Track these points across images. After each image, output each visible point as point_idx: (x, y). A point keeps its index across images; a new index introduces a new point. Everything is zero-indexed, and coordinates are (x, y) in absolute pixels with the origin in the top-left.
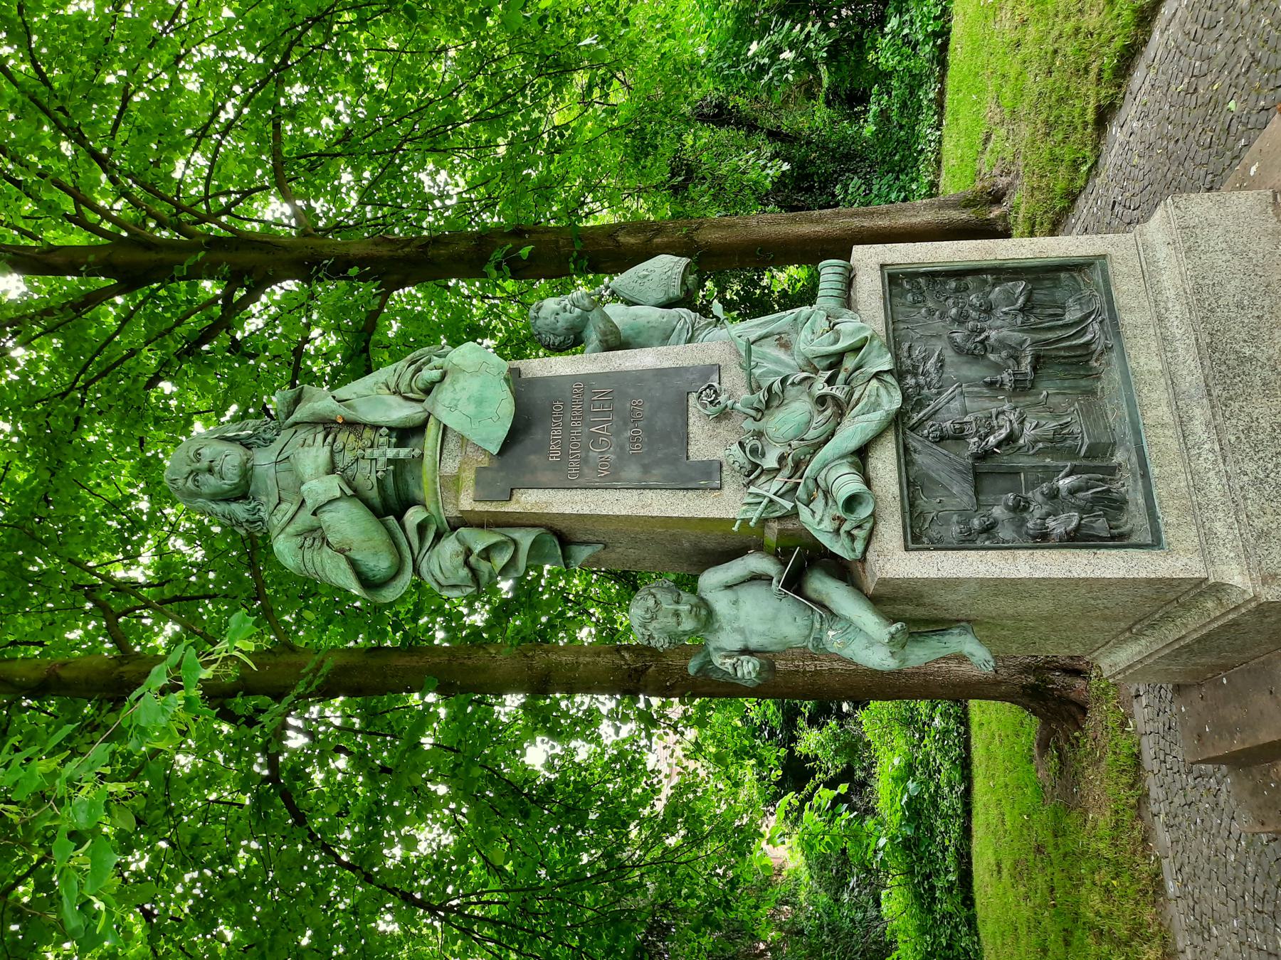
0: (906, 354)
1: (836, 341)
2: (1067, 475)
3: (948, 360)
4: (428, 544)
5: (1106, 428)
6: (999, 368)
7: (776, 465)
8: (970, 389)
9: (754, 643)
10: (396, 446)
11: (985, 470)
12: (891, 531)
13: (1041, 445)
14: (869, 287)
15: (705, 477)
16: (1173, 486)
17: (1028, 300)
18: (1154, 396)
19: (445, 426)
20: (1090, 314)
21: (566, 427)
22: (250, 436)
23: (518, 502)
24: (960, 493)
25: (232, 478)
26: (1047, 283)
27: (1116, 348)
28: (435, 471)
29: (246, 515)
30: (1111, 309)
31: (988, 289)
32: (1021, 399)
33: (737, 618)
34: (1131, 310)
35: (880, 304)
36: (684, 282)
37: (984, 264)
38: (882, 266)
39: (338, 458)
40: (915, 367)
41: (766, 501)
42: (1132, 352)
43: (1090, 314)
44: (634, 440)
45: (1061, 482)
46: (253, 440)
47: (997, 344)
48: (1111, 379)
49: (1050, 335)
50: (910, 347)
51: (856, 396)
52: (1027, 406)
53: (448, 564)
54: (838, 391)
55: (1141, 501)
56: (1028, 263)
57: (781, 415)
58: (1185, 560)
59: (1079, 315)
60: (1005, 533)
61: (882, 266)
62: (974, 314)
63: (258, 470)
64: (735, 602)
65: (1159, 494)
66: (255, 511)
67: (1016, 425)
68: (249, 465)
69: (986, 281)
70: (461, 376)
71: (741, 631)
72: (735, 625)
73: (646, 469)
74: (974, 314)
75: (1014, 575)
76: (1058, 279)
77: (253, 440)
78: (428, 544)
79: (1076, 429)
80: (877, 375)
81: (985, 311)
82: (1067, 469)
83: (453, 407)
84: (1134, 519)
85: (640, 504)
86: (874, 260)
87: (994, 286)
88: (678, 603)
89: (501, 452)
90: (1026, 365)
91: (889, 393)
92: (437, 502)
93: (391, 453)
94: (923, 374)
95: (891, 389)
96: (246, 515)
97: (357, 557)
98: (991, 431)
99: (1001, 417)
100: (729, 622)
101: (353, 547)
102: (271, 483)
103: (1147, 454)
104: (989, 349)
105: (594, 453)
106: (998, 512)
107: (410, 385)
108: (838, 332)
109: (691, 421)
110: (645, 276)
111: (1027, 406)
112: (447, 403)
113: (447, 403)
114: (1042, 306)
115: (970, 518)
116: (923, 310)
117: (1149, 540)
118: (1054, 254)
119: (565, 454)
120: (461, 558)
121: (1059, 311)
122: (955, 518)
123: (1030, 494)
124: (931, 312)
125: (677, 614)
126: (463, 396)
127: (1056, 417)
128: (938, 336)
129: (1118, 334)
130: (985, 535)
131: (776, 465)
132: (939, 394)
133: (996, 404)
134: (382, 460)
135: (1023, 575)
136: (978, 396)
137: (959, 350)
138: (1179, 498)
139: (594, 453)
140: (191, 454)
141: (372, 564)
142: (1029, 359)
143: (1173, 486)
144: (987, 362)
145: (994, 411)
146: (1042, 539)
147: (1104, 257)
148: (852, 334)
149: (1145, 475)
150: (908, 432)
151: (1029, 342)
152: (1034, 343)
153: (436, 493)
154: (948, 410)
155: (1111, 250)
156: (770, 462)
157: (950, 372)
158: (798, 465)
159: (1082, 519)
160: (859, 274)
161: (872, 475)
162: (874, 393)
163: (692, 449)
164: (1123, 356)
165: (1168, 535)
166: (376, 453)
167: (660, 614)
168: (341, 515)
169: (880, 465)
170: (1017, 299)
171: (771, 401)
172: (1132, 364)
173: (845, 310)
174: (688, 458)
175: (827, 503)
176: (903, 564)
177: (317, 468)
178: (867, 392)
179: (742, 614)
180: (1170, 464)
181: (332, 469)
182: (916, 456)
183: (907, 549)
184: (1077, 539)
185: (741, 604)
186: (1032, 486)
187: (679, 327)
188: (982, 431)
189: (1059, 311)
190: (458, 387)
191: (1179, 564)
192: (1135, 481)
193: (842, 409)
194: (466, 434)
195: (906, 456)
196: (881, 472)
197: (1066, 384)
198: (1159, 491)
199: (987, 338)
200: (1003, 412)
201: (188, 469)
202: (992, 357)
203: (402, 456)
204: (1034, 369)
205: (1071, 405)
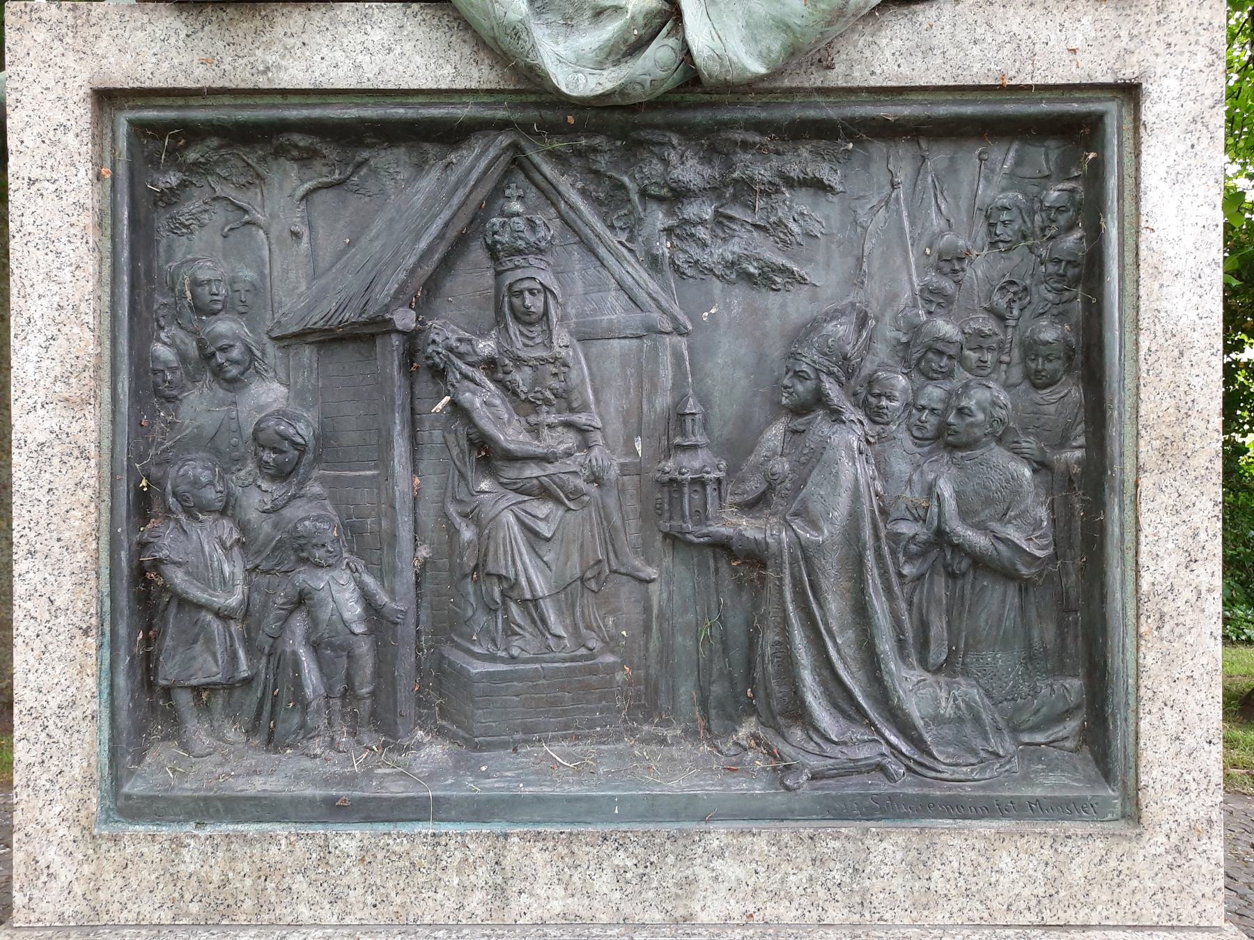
0: (794, 171)
2: (367, 598)
3: (772, 301)
5: (528, 730)
13: (467, 534)
16: (300, 884)
17: (979, 562)
18: (603, 882)
20: (917, 742)
26: (1045, 633)
27: (780, 799)
30: (925, 808)
31: (1029, 444)
32: (632, 504)
34: (918, 866)
35: (978, 71)
37: (1119, 432)
38: (1130, 92)
42: (761, 843)
43: (917, 742)
45: (344, 577)
47: (811, 440)
48: (681, 768)
49: (835, 606)
52: (605, 516)
55: (258, 785)
56: (1115, 573)
58: (65, 875)
59: (914, 709)
61: (1130, 92)
65: (273, 839)
67: (532, 471)
69: (1063, 443)
76: (1061, 670)
81: (943, 429)
82: (383, 598)
84: (217, 755)
87: (1041, 467)
98: (524, 404)
103: (405, 828)
104: (799, 423)
111: (605, 516)
114: (954, 610)
117: (134, 787)
118: (1149, 659)
121: (938, 654)
124: (951, 262)
128: (858, 277)
129: (840, 811)
130: (192, 349)
132: (654, 263)
133: (616, 427)
136: (645, 378)
138: (260, 893)
142: (750, 534)
143: (300, 884)
144: (759, 413)
146: (142, 498)
147: (1132, 813)
149: (334, 811)
151: (806, 535)
152: (806, 555)
154: (601, 286)
155: (1156, 842)
157: (727, 304)
164: (748, 813)
165: (143, 841)
170: (981, 527)
172: (719, 835)
176: (48, 79)
180: (369, 888)
184: (144, 601)
189: (938, 654)
191: (51, 855)
192: (326, 782)
197: (682, 641)
198: (284, 843)
199: (836, 415)
200: (586, 446)
202: (775, 433)
204: (722, 547)
205: (610, 643)
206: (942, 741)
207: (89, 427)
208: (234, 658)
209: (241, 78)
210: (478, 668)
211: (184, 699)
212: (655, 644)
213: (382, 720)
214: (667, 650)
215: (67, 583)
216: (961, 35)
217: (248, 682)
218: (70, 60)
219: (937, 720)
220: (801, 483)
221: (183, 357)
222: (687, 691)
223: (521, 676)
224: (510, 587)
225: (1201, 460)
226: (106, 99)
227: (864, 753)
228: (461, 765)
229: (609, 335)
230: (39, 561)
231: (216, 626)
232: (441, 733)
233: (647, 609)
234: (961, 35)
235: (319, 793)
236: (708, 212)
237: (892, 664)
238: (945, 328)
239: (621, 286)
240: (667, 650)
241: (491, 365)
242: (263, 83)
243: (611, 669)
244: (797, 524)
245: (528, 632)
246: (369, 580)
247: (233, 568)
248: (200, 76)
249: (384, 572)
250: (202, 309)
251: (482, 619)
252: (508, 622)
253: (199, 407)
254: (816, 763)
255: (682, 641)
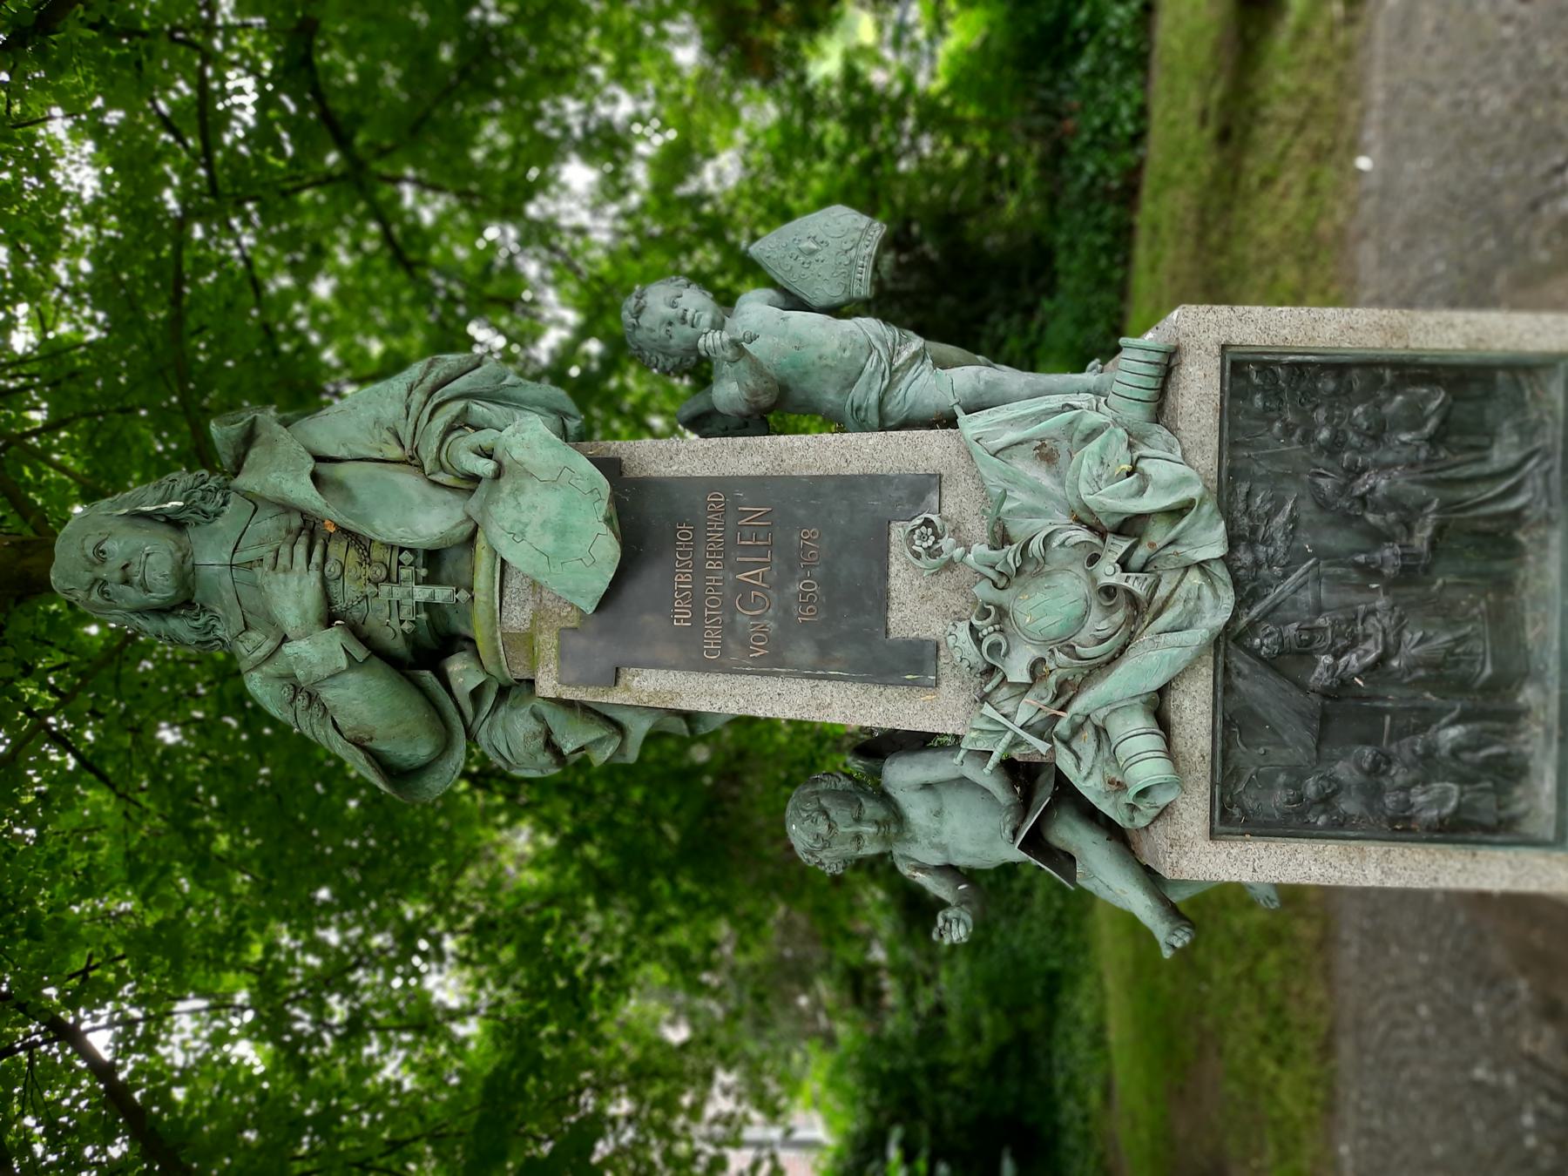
0: (1241, 506)
1: (1141, 492)
2: (1453, 723)
4: (487, 708)
6: (1378, 537)
7: (1026, 679)
8: (1331, 570)
9: (959, 861)
10: (427, 581)
11: (1341, 711)
12: (1194, 810)
13: (1421, 673)
14: (1200, 386)
15: (914, 663)
17: (1444, 421)
19: (503, 561)
21: (699, 572)
22: (179, 510)
23: (628, 688)
24: (1296, 744)
25: (163, 589)
28: (493, 624)
29: (195, 637)
31: (1382, 395)
33: (938, 832)
36: (876, 269)
38: (1224, 347)
39: (335, 588)
40: (1254, 530)
41: (1009, 736)
44: (806, 599)
46: (187, 514)
50: (1248, 494)
51: (1163, 592)
53: (521, 750)
54: (1137, 585)
57: (1039, 597)
59: (1514, 457)
60: (1349, 805)
61: (1224, 347)
62: (1354, 439)
63: (203, 572)
64: (938, 813)
66: (209, 629)
67: (1391, 639)
68: (188, 565)
69: (1381, 379)
70: (527, 483)
71: (943, 848)
72: (936, 840)
73: (824, 649)
74: (1354, 439)
75: (1359, 882)
77: (187, 514)
78: (487, 708)
79: (1478, 646)
80: (1201, 566)
81: (1374, 438)
82: (1454, 715)
83: (518, 535)
85: (814, 703)
86: (1213, 335)
88: (858, 820)
89: (599, 609)
90: (1421, 538)
91: (1216, 596)
92: (499, 661)
93: (422, 593)
94: (1264, 542)
95: (1219, 585)
96: (195, 637)
97: (383, 748)
99: (1372, 620)
100: (927, 835)
101: (377, 733)
102: (228, 597)
105: (744, 617)
106: (1343, 770)
107: (438, 459)
108: (1144, 477)
109: (893, 570)
110: (812, 252)
112: (507, 525)
113: (507, 525)
115: (1303, 778)
116: (1278, 425)
119: (697, 617)
120: (541, 740)
122: (1282, 778)
123: (1394, 748)
124: (1288, 431)
125: (858, 837)
126: (536, 518)
127: (1451, 624)
130: (1321, 807)
131: (1026, 679)
132: (1286, 576)
133: (1365, 597)
134: (408, 604)
135: (1372, 883)
136: (1339, 582)
137: (1323, 505)
139: (744, 617)
140: (90, 552)
141: (406, 754)
145: (1362, 608)
146: (1401, 828)
148: (1170, 487)
150: (1232, 646)
151: (1434, 505)
153: (497, 653)
154: (1294, 604)
156: (1018, 671)
158: (1065, 692)
159: (1462, 794)
160: (1187, 360)
161: (1174, 718)
162: (1193, 595)
163: (894, 617)
166: (398, 592)
167: (835, 841)
168: (351, 693)
169: (1187, 703)
170: (1426, 419)
171: (1028, 567)
173: (1156, 427)
174: (887, 632)
175: (1099, 748)
176: (1205, 860)
177: (304, 613)
178: (1181, 592)
179: (947, 829)
181: (328, 620)
182: (1239, 683)
183: (1213, 835)
184: (1456, 830)
185: (946, 816)
186: (1398, 734)
187: (869, 369)
188: (1341, 643)
190: (525, 500)
192: (1548, 743)
193: (1139, 610)
194: (541, 579)
195: (1224, 687)
196: (1187, 715)
201: (88, 577)
202: (1371, 518)
203: (439, 600)
204: (1433, 544)
206: (1530, 443)
207: (1374, 849)
208: (1481, 790)
209: (1206, 768)
210: (1488, 671)
211: (1503, 814)
212: (1476, 581)
213: (1514, 716)
214: (1479, 575)
215: (1451, 863)
216: (1195, 428)
217: (1495, 783)
218: (1196, 850)
219: (1520, 446)
220: (1404, 507)
221: (1324, 812)
222: (1499, 566)
223: (1493, 649)
224: (1450, 652)
225: (1403, 320)
226: (1213, 835)
227: (1539, 482)
228: (1539, 678)
229: (1318, 599)
230: (1440, 876)
231: (1468, 796)
232: (1519, 689)
233: (1458, 584)
234: (1195, 428)
235: (1555, 747)
236: (1262, 548)
237: (1486, 469)
238: (1324, 434)
239: (1295, 592)
240: (1479, 575)
241: (1337, 657)
242: (1208, 758)
243: (1488, 604)
244: (1426, 511)
245: (1470, 644)
246: (1444, 721)
247: (1437, 787)
248: (1204, 786)
249: (1441, 713)
250: (1300, 799)
251: (1463, 666)
252: (1465, 653)
253: (1349, 805)
254: (1544, 505)
255: (1474, 568)
